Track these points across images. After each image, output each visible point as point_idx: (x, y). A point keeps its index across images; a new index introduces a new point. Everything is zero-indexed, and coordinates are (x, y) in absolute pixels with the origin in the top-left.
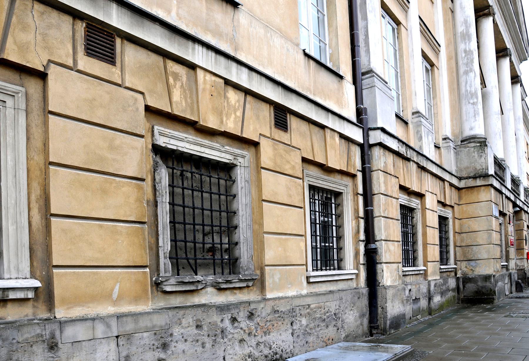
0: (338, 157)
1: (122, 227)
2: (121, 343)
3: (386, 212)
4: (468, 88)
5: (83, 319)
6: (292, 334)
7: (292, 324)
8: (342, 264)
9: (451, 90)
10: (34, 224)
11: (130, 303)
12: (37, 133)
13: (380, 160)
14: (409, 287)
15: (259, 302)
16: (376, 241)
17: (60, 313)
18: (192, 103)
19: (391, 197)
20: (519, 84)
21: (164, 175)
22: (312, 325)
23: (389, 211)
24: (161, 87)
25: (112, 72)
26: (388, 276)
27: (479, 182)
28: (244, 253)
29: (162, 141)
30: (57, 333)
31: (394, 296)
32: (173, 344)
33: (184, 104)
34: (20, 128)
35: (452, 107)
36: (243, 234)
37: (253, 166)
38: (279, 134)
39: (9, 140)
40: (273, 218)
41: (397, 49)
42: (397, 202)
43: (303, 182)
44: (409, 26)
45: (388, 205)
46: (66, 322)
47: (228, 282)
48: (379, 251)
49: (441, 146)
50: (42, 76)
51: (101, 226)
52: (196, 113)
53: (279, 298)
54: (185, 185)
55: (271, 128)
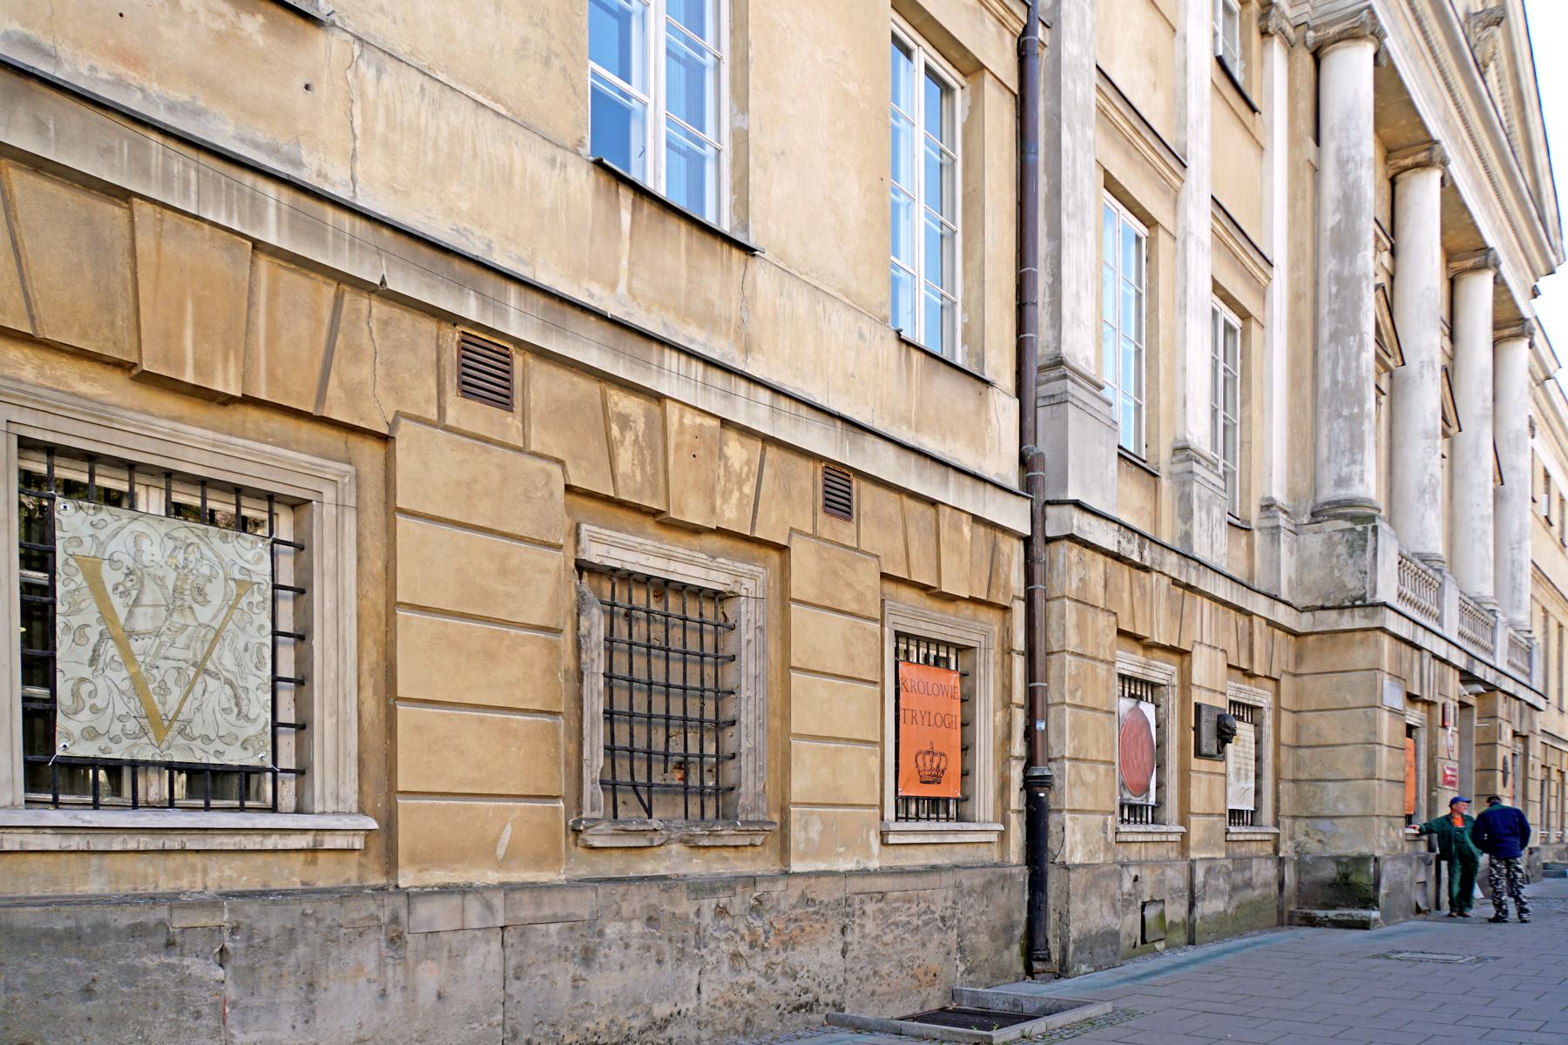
0: (968, 567)
1: (518, 721)
2: (509, 941)
3: (1079, 694)
4: (1340, 377)
5: (446, 890)
6: (844, 953)
7: (843, 931)
8: (966, 808)
9: (1295, 383)
10: (366, 715)
11: (527, 868)
12: (375, 548)
13: (1073, 572)
14: (1134, 871)
15: (772, 879)
16: (1050, 760)
17: (407, 878)
18: (655, 475)
19: (1094, 659)
20: (1527, 341)
21: (596, 624)
22: (888, 938)
23: (1085, 692)
24: (596, 447)
25: (505, 425)
26: (1076, 840)
27: (1346, 621)
28: (749, 779)
29: (594, 553)
30: (403, 914)
31: (1093, 885)
32: (603, 951)
33: (639, 478)
34: (347, 542)
35: (1294, 424)
36: (747, 738)
37: (775, 594)
38: (832, 527)
39: (329, 562)
40: (818, 706)
41: (1144, 292)
42: (1109, 671)
43: (882, 626)
44: (1180, 230)
45: (1085, 679)
46: (417, 894)
47: (712, 834)
48: (1057, 782)
49: (1254, 524)
50: (386, 439)
51: (481, 721)
52: (662, 493)
53: (819, 874)
54: (1356, 808)
55: (815, 514)
